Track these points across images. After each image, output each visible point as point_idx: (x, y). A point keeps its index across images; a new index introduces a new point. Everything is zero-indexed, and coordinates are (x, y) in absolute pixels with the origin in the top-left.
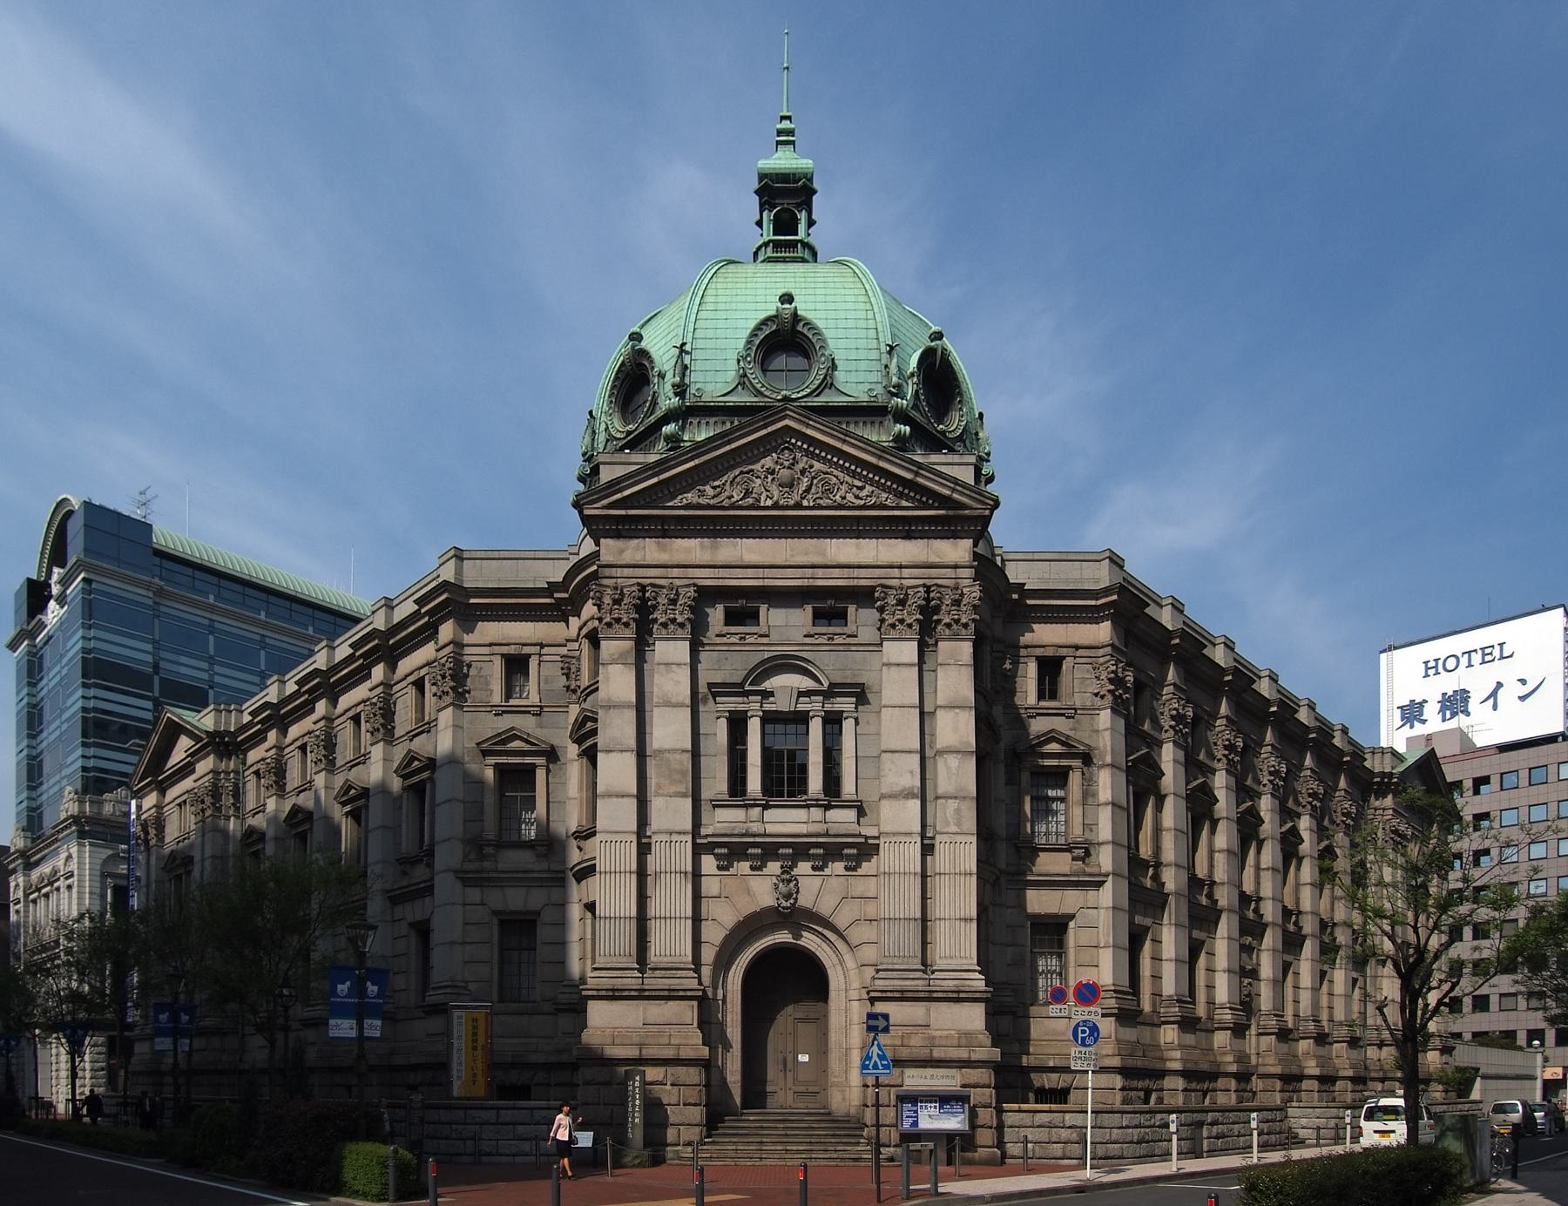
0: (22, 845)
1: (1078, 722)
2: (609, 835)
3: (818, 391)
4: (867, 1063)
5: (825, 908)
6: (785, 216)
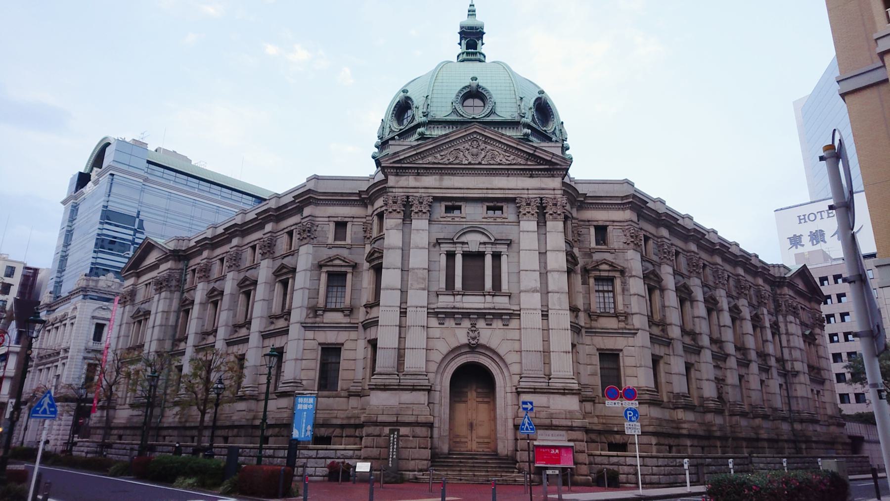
0: (48, 300)
3: (488, 115)
5: (493, 345)
6: (471, 42)
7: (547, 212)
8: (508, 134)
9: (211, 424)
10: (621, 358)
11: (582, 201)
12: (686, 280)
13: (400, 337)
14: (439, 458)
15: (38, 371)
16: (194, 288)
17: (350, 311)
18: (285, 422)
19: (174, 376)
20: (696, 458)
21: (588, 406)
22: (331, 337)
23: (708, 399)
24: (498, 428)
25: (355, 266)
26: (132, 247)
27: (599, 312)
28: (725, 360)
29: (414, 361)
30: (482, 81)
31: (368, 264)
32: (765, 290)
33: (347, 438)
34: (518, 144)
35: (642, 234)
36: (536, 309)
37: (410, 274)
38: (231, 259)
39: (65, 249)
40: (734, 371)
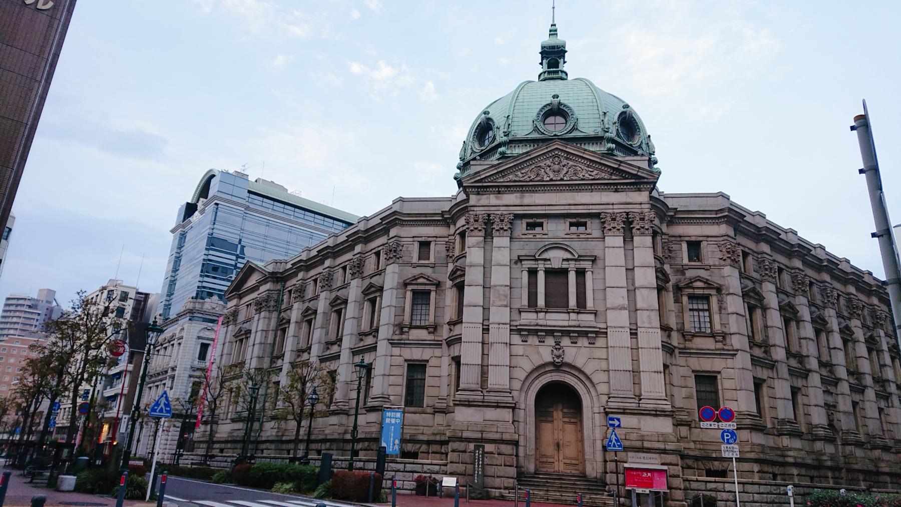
3: (570, 132)
5: (579, 363)
7: (634, 227)
8: (591, 149)
9: (306, 438)
10: (719, 381)
11: (673, 215)
12: (791, 299)
13: (483, 354)
14: (525, 477)
15: (148, 389)
16: (290, 308)
17: (434, 328)
18: (373, 436)
19: (272, 391)
20: (803, 487)
21: (684, 431)
22: (417, 354)
23: (816, 426)
25: (438, 285)
26: (235, 271)
27: (693, 331)
28: (836, 385)
29: (498, 378)
30: (563, 98)
31: (451, 282)
32: (881, 310)
33: (433, 455)
34: (601, 159)
35: (739, 250)
37: (492, 290)
38: (324, 280)
39: (174, 274)
40: (847, 396)
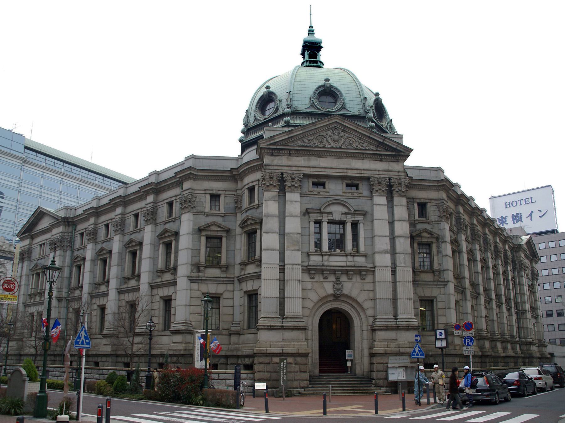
1: (433, 226)
2: (268, 265)
4: (78, 340)
5: (354, 294)
16: (84, 248)
18: (182, 353)
22: (212, 288)
24: (356, 356)
25: (228, 231)
33: (231, 366)
36: (387, 267)
